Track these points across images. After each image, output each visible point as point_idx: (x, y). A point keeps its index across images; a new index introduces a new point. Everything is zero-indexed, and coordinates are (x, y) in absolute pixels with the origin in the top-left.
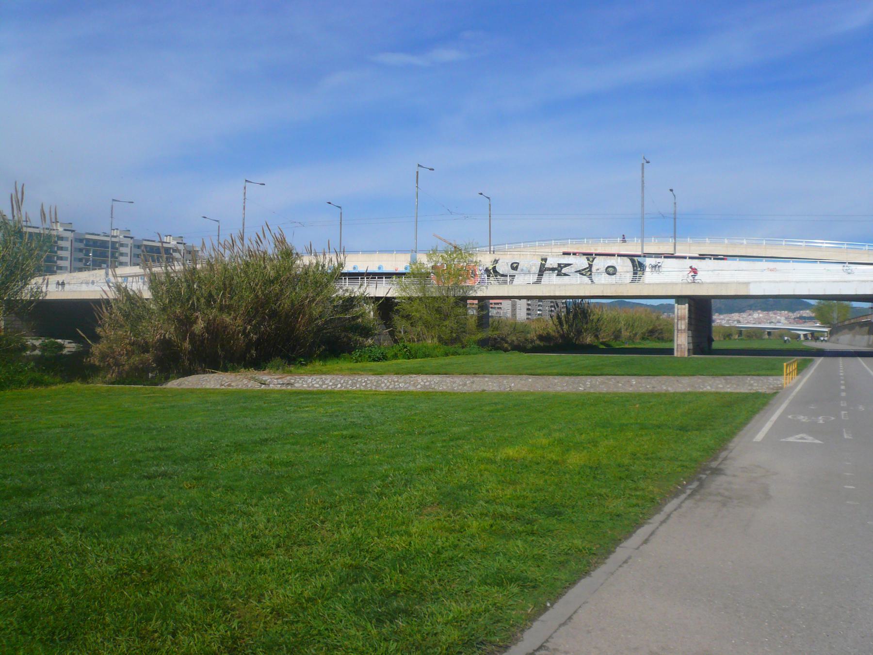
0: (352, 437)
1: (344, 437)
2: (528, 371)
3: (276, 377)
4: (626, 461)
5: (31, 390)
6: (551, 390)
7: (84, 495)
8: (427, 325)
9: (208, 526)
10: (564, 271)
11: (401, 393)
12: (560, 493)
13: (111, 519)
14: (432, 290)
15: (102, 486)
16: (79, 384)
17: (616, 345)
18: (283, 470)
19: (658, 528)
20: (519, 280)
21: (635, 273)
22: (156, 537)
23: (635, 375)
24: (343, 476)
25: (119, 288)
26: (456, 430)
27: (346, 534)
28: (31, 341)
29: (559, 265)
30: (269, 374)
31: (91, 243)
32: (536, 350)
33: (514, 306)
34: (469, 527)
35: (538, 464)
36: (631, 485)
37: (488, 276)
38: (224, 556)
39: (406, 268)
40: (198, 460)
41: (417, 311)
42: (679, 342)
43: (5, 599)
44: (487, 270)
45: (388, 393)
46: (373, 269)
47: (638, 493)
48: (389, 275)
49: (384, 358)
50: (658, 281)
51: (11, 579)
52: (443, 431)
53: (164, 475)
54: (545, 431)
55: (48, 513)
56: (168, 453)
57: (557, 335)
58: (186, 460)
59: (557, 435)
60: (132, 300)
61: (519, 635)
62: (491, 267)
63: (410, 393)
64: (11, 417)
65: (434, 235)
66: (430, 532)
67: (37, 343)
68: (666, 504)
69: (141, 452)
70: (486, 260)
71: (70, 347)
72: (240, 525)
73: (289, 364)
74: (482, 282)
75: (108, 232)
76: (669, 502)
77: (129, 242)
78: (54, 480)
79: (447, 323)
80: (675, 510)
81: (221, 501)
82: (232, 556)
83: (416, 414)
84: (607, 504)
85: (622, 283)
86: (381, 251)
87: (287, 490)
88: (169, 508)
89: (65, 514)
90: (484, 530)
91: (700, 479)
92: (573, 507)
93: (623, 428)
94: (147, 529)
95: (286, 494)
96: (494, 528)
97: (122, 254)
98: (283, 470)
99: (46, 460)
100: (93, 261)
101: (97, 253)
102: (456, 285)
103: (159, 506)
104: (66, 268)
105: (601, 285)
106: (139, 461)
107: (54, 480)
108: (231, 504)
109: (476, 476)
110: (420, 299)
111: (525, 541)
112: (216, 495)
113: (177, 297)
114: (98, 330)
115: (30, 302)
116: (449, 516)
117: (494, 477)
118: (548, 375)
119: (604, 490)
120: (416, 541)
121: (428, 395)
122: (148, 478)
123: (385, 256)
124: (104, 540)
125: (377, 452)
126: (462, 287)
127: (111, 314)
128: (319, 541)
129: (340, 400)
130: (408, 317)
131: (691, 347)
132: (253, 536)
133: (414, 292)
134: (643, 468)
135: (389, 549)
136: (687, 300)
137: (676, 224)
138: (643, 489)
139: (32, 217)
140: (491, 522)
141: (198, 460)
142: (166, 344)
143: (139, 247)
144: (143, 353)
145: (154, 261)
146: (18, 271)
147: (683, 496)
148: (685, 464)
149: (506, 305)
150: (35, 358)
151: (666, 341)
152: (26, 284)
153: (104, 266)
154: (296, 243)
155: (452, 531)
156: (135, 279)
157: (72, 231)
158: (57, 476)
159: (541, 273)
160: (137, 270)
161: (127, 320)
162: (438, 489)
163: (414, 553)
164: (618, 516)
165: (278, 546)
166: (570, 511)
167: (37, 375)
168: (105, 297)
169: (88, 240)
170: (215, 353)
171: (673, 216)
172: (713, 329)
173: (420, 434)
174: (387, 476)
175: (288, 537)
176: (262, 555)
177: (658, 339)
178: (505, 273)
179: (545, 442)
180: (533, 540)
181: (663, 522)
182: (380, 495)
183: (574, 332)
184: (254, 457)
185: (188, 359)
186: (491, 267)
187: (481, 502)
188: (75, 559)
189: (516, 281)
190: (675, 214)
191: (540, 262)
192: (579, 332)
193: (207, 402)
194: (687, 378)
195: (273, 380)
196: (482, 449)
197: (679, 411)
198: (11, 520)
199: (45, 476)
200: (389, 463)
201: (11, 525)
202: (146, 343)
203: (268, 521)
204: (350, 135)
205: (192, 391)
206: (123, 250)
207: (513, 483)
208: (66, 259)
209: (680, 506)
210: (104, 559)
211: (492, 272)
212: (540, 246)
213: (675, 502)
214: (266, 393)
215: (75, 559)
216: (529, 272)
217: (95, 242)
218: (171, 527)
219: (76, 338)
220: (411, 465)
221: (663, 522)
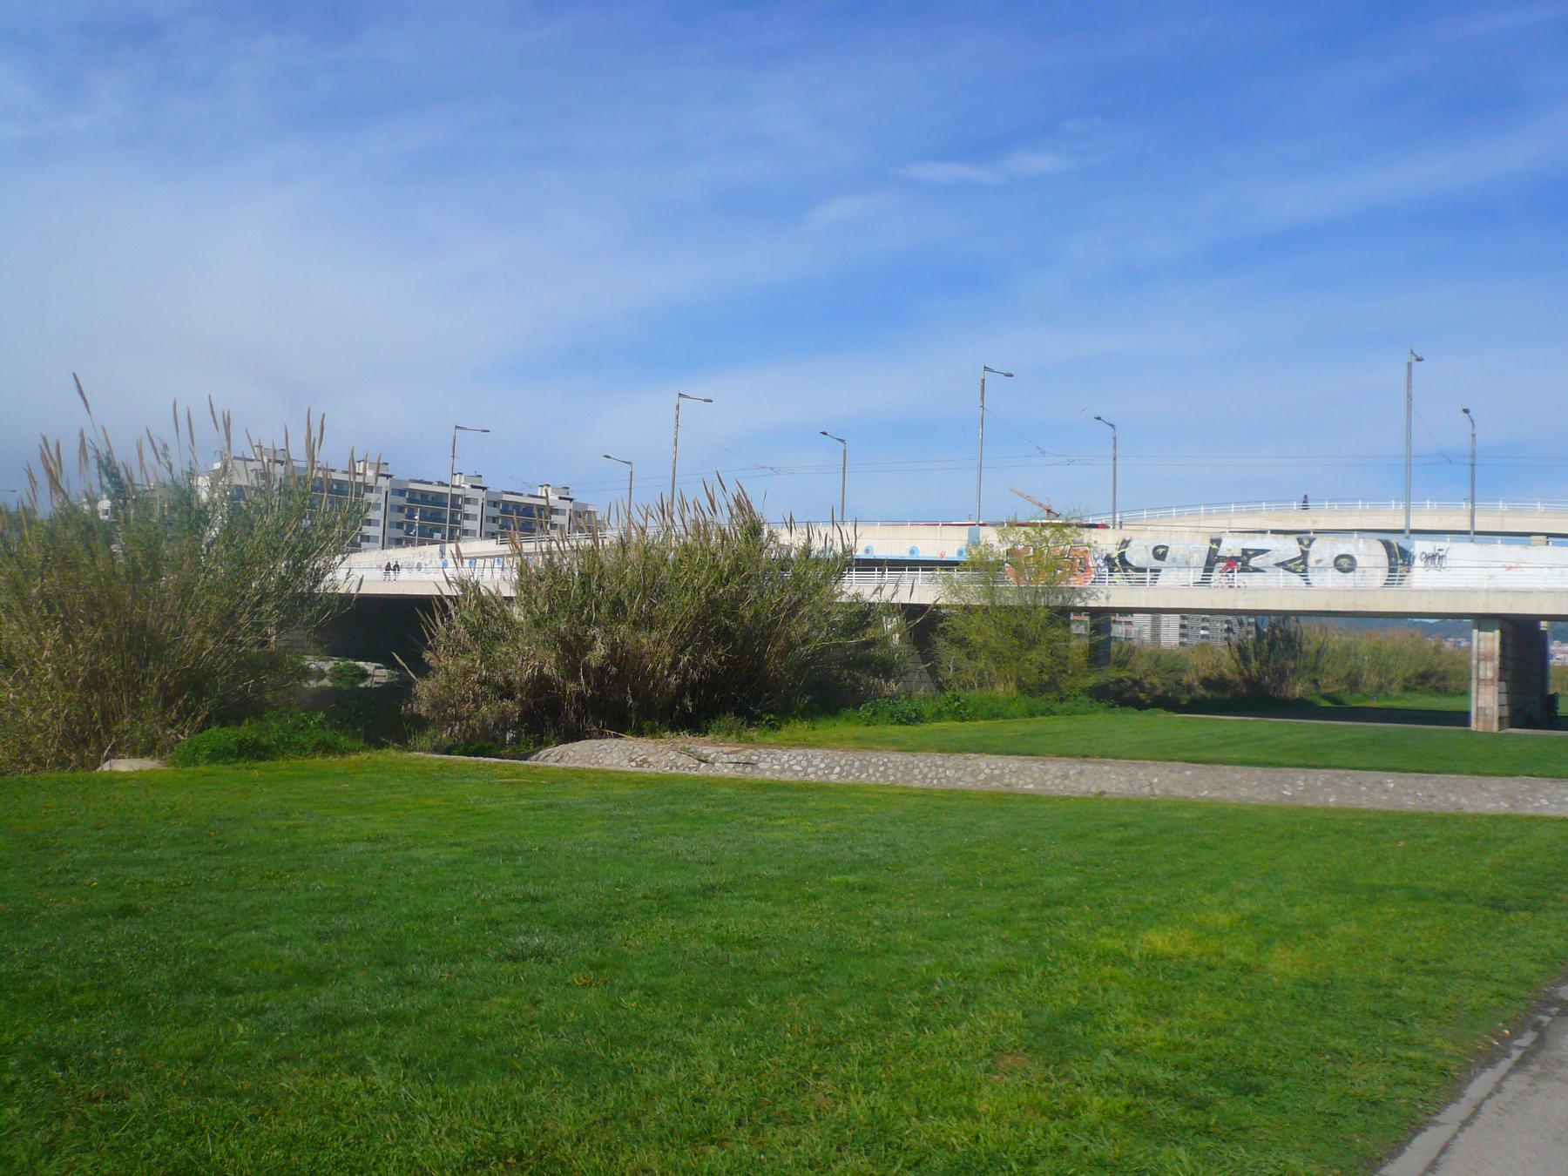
0: (864, 889)
1: (850, 887)
2: (1186, 755)
3: (727, 749)
4: (1385, 975)
6: (1228, 795)
8: (997, 657)
9: (616, 1072)
10: (1254, 562)
11: (950, 794)
12: (1257, 1042)
14: (1008, 594)
15: (437, 972)
16: (393, 753)
17: (1353, 701)
18: (740, 955)
19: (1455, 1137)
20: (1167, 578)
21: (1391, 571)
22: (528, 1090)
23: (1394, 770)
24: (851, 976)
25: (506, 678)
26: (1054, 882)
27: (859, 1106)
28: (312, 663)
29: (1245, 551)
30: (714, 743)
31: (418, 497)
32: (1197, 706)
33: (1156, 628)
34: (1085, 1107)
35: (1210, 969)
36: (1397, 1032)
37: (1111, 570)
38: (646, 1139)
39: (960, 553)
40: (595, 924)
41: (978, 631)
42: (1481, 703)
44: (1108, 560)
45: (926, 793)
46: (904, 554)
47: (1412, 1054)
48: (928, 565)
49: (916, 718)
50: (1437, 585)
52: (1029, 884)
53: (539, 954)
54: (1223, 894)
55: (347, 1023)
56: (544, 908)
57: (1237, 678)
58: (575, 924)
59: (1245, 905)
60: (487, 605)
62: (1115, 554)
63: (964, 795)
64: (287, 815)
65: (1012, 490)
66: (1015, 1115)
67: (327, 666)
68: (1470, 1081)
69: (500, 903)
70: (1106, 542)
71: (377, 674)
72: (672, 1074)
73: (749, 725)
74: (1100, 579)
76: (1477, 1075)
77: (480, 495)
79: (1033, 655)
80: (1490, 1096)
81: (637, 1017)
82: (660, 1140)
83: (979, 844)
84: (1349, 1073)
85: (1367, 588)
86: (915, 523)
87: (752, 1001)
88: (550, 1026)
89: (379, 1028)
90: (1113, 1117)
91: (1537, 1026)
92: (1284, 1078)
93: (1376, 894)
94: (514, 1070)
95: (749, 1008)
96: (1132, 1113)
97: (467, 517)
98: (740, 955)
99: (344, 910)
101: (428, 515)
102: (1052, 588)
103: (532, 1022)
105: (1325, 591)
106: (498, 923)
108: (655, 1025)
109: (1095, 992)
110: (986, 610)
111: (1193, 1150)
112: (630, 1003)
113: (560, 601)
114: (427, 655)
116: (1047, 1079)
117: (1130, 998)
118: (1224, 762)
119: (1344, 1042)
120: (986, 1128)
121: (1003, 802)
122: (513, 959)
123: (924, 531)
124: (444, 1088)
125: (911, 924)
126: (1061, 591)
128: (812, 1117)
129: (840, 805)
130: (961, 643)
131: (1506, 713)
132: (696, 1100)
133: (973, 595)
134: (1421, 995)
135: (940, 1145)
136: (1497, 622)
137: (1472, 472)
138: (1421, 1045)
139: (333, 459)
140: (1127, 1099)
141: (595, 924)
142: (540, 684)
143: (495, 504)
144: (501, 698)
146: (307, 551)
147: (1505, 1064)
148: (1509, 990)
149: (1142, 621)
151: (1453, 695)
153: (437, 536)
154: (769, 511)
155: (1054, 1115)
157: (388, 476)
159: (1209, 566)
160: (491, 546)
161: (476, 639)
162: (1025, 1016)
163: (985, 1160)
164: (1375, 1103)
165: (739, 1123)
166: (1278, 1084)
167: (328, 735)
170: (623, 703)
171: (1468, 460)
172: (1551, 671)
173: (987, 886)
174: (931, 982)
175: (756, 1105)
176: (712, 1142)
177: (1437, 690)
178: (1142, 565)
179: (1223, 919)
180: (1209, 1149)
181: (1466, 1123)
182: (920, 1023)
183: (1269, 678)
184: (692, 925)
185: (576, 712)
186: (1115, 554)
187: (1108, 1053)
188: (396, 1126)
189: (1163, 579)
190: (1473, 456)
191: (1207, 546)
192: (1281, 675)
193: (607, 799)
194: (1498, 780)
195: (717, 758)
196: (1106, 929)
197: (1487, 861)
198: (291, 1033)
199: (345, 944)
200: (933, 951)
201: (291, 1043)
202: (509, 684)
203: (721, 1067)
204: (858, 309)
205: (580, 774)
206: (469, 509)
207: (1166, 1010)
208: (377, 523)
209: (1498, 1089)
211: (1119, 563)
212: (1208, 514)
213: (1487, 1078)
214: (710, 784)
215: (396, 1126)
216: (1187, 565)
218: (554, 1069)
219: (390, 664)
220: (975, 959)
221: (1466, 1123)
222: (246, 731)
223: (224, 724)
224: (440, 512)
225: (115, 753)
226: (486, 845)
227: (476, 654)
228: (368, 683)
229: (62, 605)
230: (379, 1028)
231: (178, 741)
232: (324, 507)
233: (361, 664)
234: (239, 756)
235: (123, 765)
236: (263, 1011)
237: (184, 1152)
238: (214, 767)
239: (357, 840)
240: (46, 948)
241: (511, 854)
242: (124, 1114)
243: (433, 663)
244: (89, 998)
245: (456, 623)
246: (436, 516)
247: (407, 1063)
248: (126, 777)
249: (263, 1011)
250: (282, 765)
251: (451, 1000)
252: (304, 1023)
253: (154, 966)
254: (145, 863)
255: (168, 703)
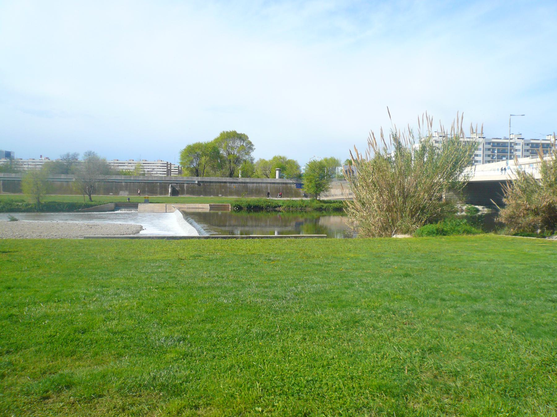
5: (465, 236)
7: (510, 306)
13: (532, 325)
25: (519, 173)
31: (496, 144)
43: (473, 362)
51: (474, 350)
55: (488, 314)
60: (527, 180)
61: (63, 315)
64: (456, 252)
67: (464, 208)
69: (544, 283)
71: (483, 210)
75: (508, 137)
77: (521, 141)
78: (489, 294)
99: (482, 280)
100: (498, 156)
101: (500, 150)
104: (480, 161)
106: (544, 289)
107: (489, 294)
114: (504, 200)
115: (464, 183)
127: (513, 190)
143: (528, 144)
145: (432, 149)
150: (463, 217)
152: (461, 172)
153: (504, 158)
156: (532, 167)
158: (491, 292)
161: (524, 193)
168: (509, 179)
169: (532, 144)
206: (517, 147)
208: (480, 155)
210: (531, 352)
217: (498, 144)
219: (488, 205)
222: (439, 225)
223: (431, 223)
224: (505, 149)
225: (396, 232)
226: (535, 265)
227: (525, 199)
228: (480, 213)
229: (379, 184)
230: (501, 317)
231: (416, 229)
232: (459, 153)
233: (477, 207)
234: (437, 234)
235: (400, 236)
236: (457, 307)
237: (436, 342)
238: (429, 237)
239: (483, 261)
240: (384, 283)
241: (546, 268)
242: (415, 329)
243: (507, 203)
244: (400, 297)
245: (516, 187)
246: (504, 151)
247: (513, 329)
248: (401, 239)
249: (457, 307)
250: (452, 237)
251: (528, 312)
252: (472, 312)
253: (418, 291)
254: (411, 263)
255: (412, 216)
